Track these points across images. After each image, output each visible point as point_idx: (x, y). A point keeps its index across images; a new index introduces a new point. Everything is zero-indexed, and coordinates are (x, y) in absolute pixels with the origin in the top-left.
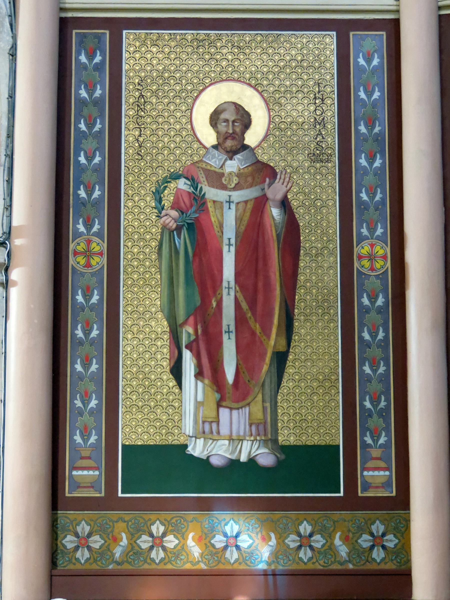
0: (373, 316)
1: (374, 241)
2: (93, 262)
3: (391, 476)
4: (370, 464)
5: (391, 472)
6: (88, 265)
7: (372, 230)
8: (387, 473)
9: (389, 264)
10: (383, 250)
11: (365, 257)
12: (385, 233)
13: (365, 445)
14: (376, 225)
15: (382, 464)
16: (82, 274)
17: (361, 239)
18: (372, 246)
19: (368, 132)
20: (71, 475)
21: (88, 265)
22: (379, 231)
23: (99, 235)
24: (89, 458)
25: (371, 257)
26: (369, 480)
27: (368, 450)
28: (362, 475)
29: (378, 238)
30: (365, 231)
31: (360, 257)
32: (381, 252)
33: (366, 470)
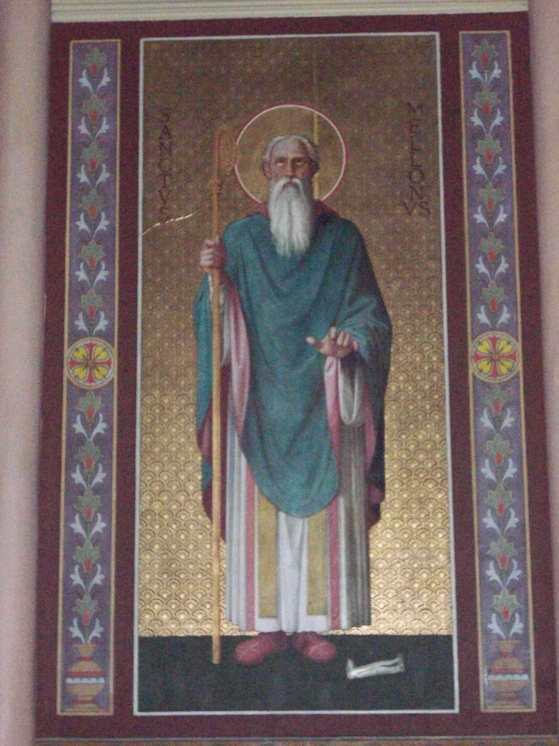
0: (500, 444)
1: (498, 334)
2: (503, 369)
3: (106, 685)
4: (498, 664)
5: (530, 676)
6: (495, 373)
7: (493, 314)
8: (102, 680)
9: (519, 367)
10: (510, 344)
11: (483, 357)
12: (110, 328)
13: (70, 641)
14: (500, 309)
15: (515, 664)
16: (83, 392)
17: (76, 335)
18: (494, 341)
19: (91, 181)
20: (64, 685)
21: (495, 373)
22: (102, 325)
23: (507, 328)
24: (91, 659)
25: (494, 358)
26: (75, 691)
27: (75, 646)
28: (64, 685)
29: (100, 334)
30: (81, 325)
31: (478, 357)
32: (507, 349)
33: (69, 677)
